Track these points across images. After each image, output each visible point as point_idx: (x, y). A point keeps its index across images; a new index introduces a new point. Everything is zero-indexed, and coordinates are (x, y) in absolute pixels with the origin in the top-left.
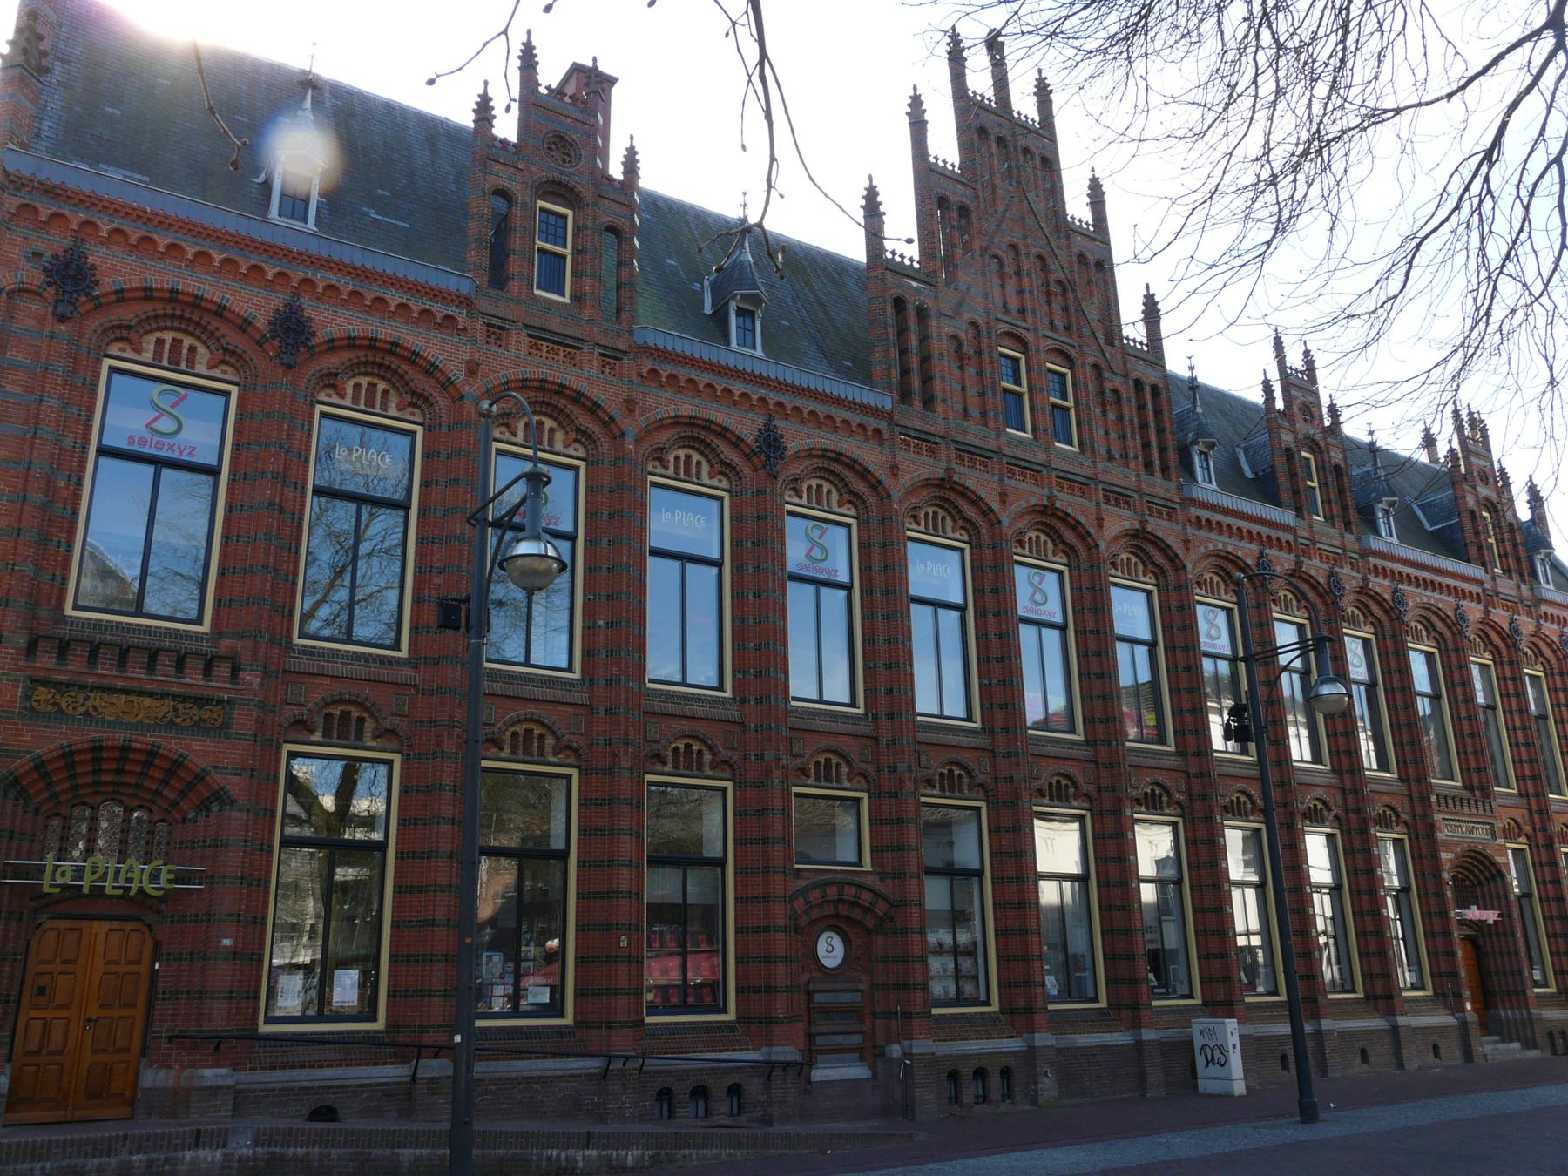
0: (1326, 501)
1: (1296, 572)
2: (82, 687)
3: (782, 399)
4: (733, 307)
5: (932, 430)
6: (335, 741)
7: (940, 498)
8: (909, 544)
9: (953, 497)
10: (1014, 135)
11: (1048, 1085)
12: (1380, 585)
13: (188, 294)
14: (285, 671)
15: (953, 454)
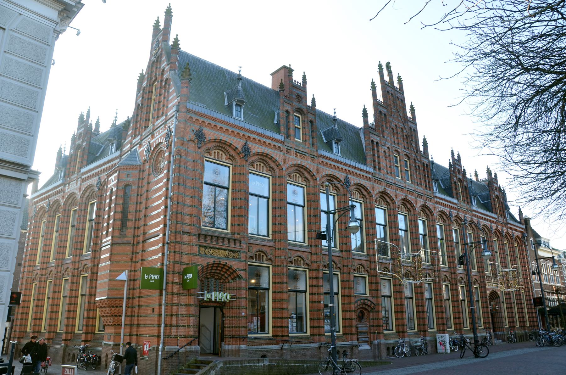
0: (463, 196)
1: (457, 216)
2: (210, 248)
4: (234, 103)
8: (206, 163)
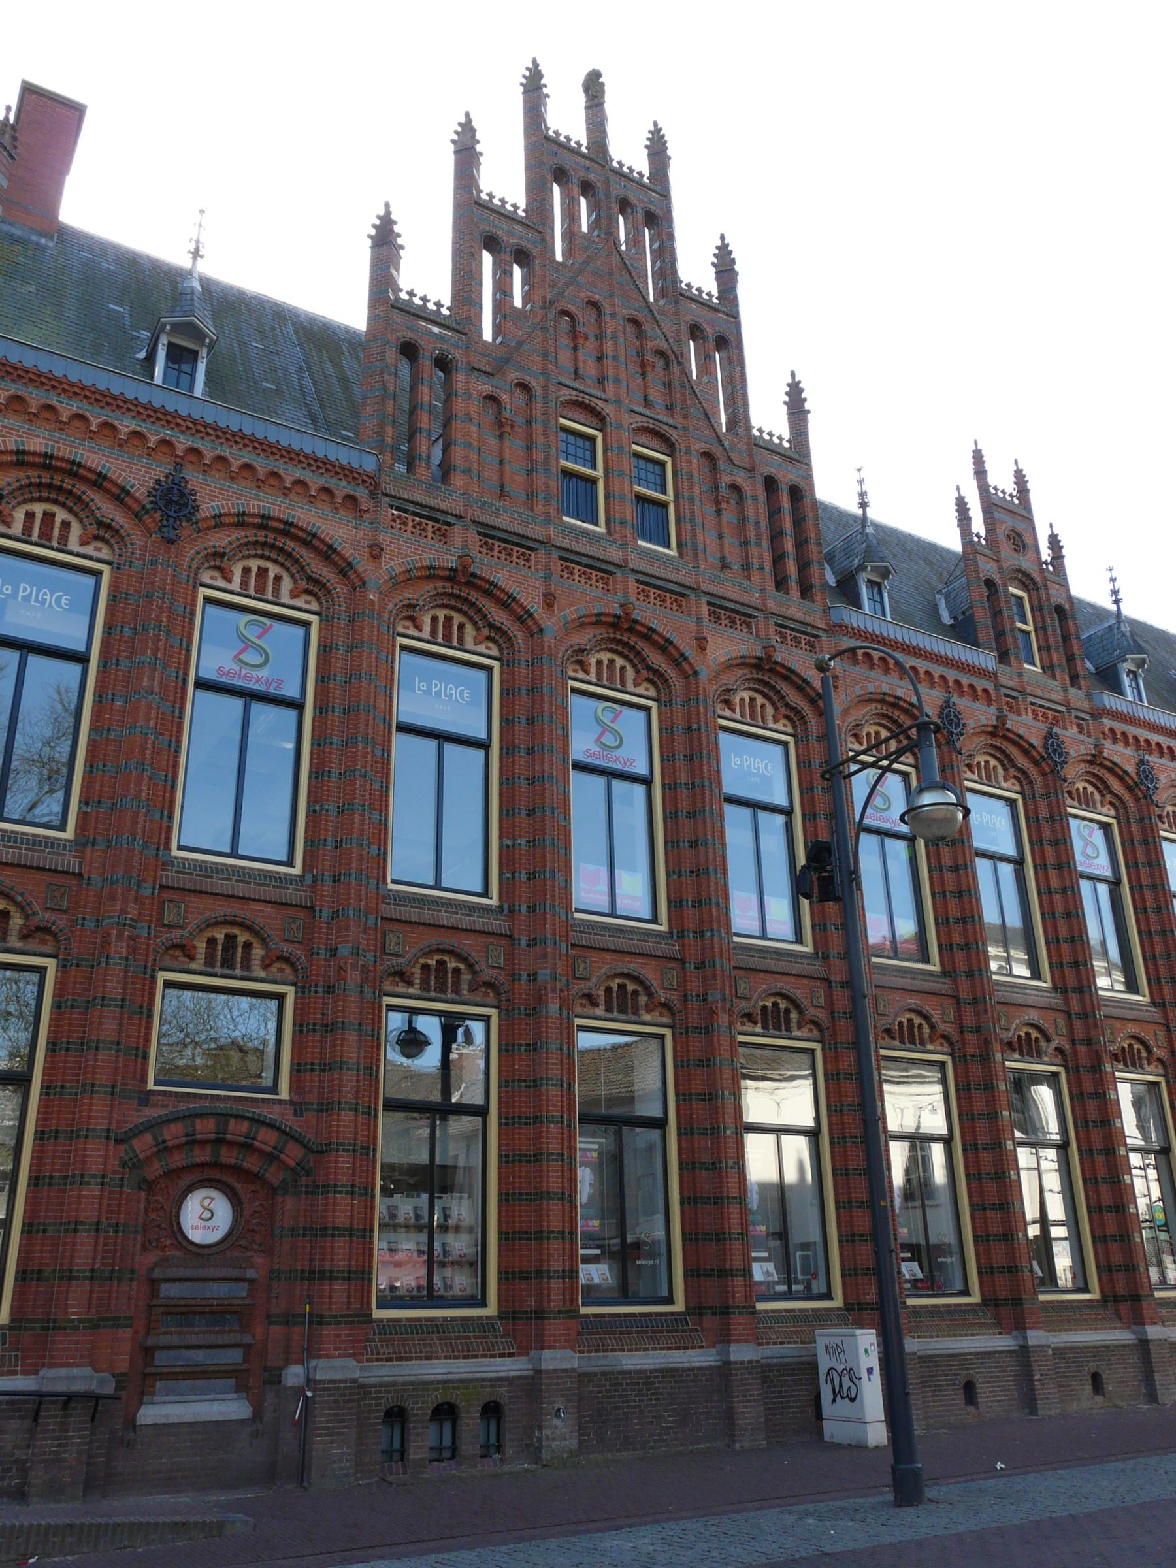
0: (1044, 648)
3: (199, 445)
5: (443, 506)
6: (218, 970)
7: (760, 681)
9: (474, 596)
10: (607, 182)
11: (560, 1431)
12: (1122, 755)
13: (62, 459)
14: (161, 886)
15: (705, 610)
